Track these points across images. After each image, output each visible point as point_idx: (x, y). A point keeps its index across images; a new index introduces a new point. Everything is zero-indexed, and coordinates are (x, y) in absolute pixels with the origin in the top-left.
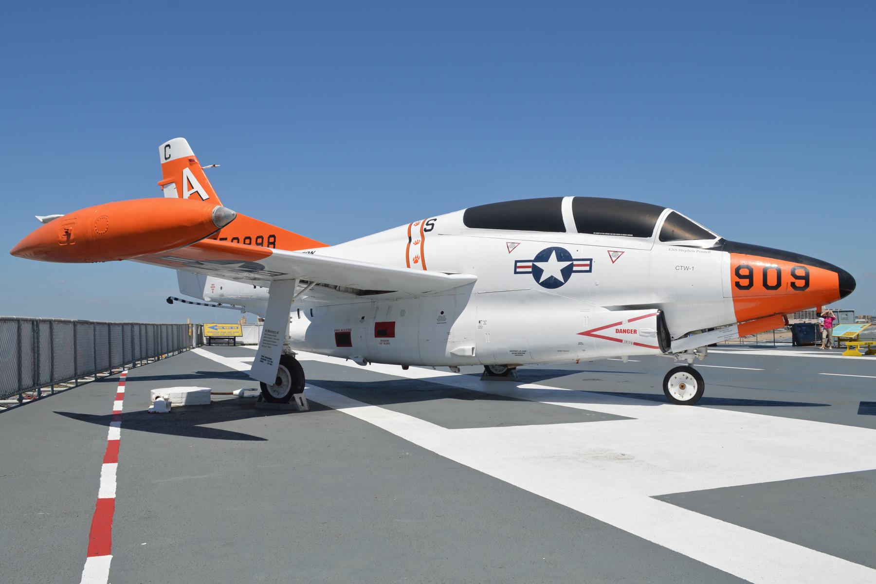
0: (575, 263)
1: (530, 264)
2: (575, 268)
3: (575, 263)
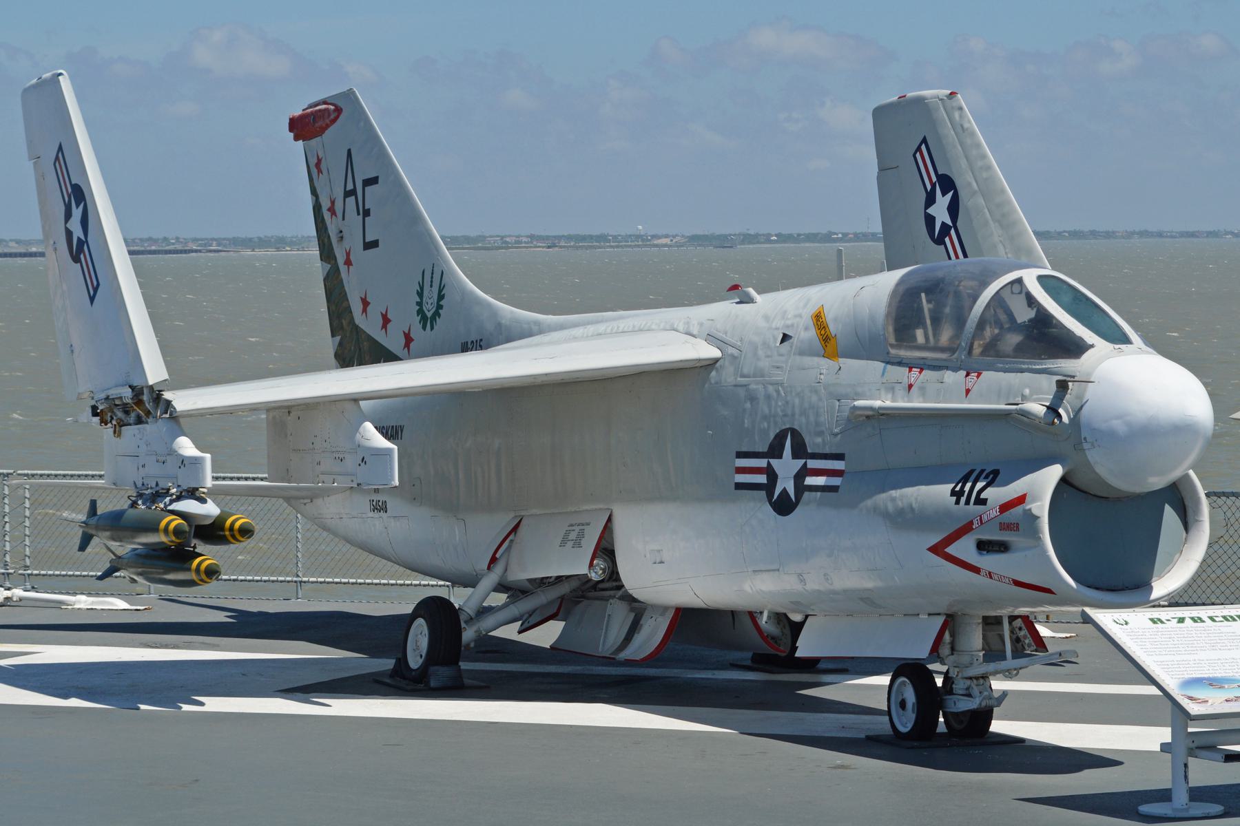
0: (813, 464)
1: (762, 463)
2: (810, 481)
3: (813, 464)
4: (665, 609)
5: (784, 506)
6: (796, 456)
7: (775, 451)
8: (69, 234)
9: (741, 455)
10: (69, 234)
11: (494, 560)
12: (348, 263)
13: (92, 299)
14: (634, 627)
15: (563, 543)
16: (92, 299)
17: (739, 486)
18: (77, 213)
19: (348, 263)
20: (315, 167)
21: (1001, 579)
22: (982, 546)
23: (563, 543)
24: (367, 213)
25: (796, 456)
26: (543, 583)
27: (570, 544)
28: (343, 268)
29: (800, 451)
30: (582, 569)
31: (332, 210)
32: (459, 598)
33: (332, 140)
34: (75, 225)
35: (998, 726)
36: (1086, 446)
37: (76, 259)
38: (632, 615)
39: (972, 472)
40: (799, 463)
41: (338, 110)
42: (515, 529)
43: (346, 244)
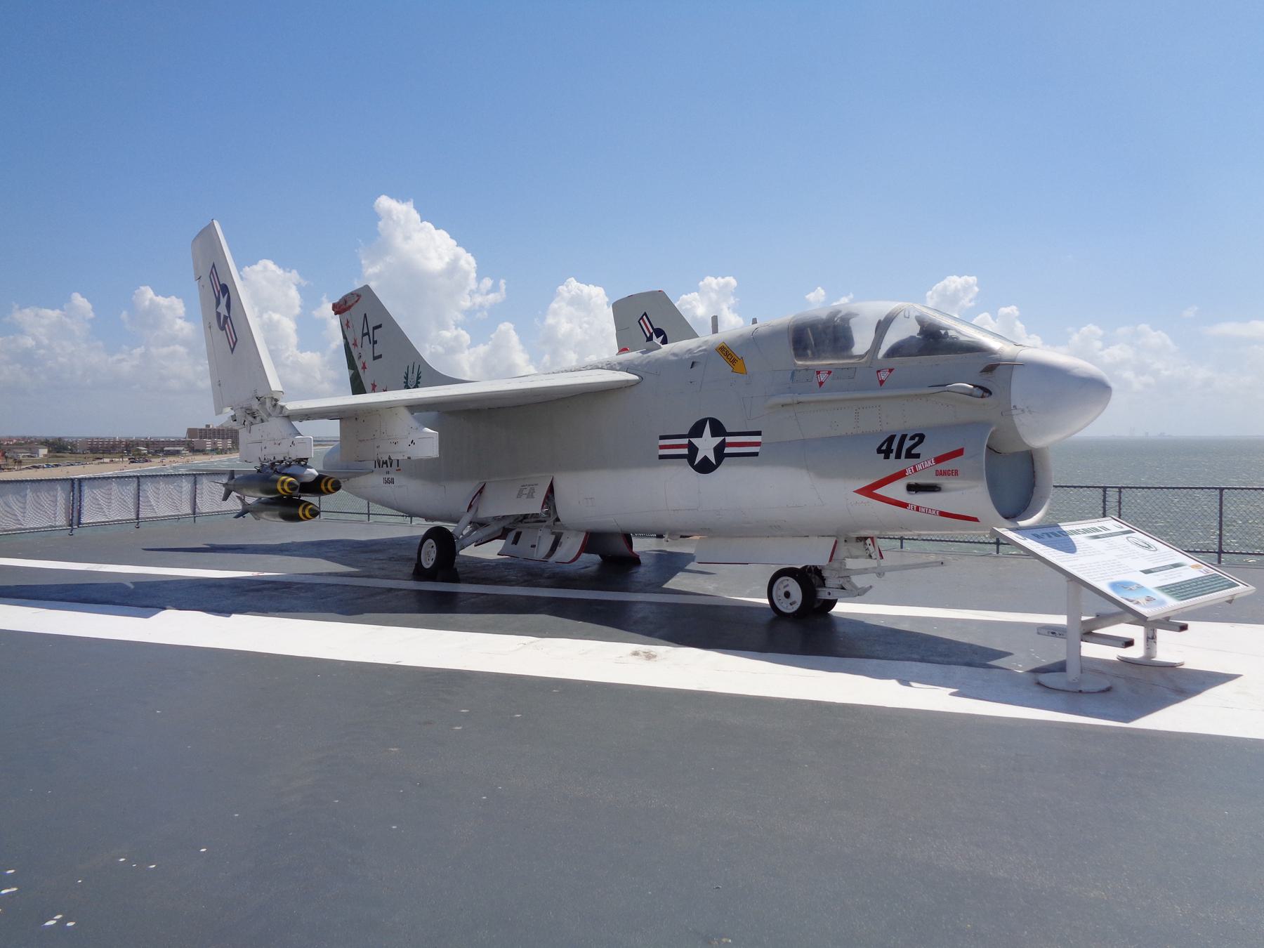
0: (729, 439)
2: (727, 450)
4: (579, 531)
5: (705, 467)
6: (714, 434)
7: (697, 431)
8: (218, 315)
9: (662, 438)
10: (218, 315)
11: (470, 506)
12: (364, 368)
13: (232, 350)
14: (556, 544)
15: (519, 496)
16: (232, 350)
17: (662, 457)
18: (223, 301)
19: (364, 368)
20: (345, 326)
21: (927, 511)
22: (912, 488)
23: (519, 496)
24: (375, 342)
25: (714, 434)
26: (497, 519)
27: (893, 455)
28: (361, 371)
29: (718, 429)
30: (538, 510)
31: (355, 345)
32: (451, 527)
33: (355, 314)
34: (223, 310)
35: (842, 608)
36: (1014, 412)
37: (223, 328)
38: (553, 537)
39: (891, 439)
40: (719, 440)
41: (359, 296)
42: (480, 492)
43: (363, 359)
